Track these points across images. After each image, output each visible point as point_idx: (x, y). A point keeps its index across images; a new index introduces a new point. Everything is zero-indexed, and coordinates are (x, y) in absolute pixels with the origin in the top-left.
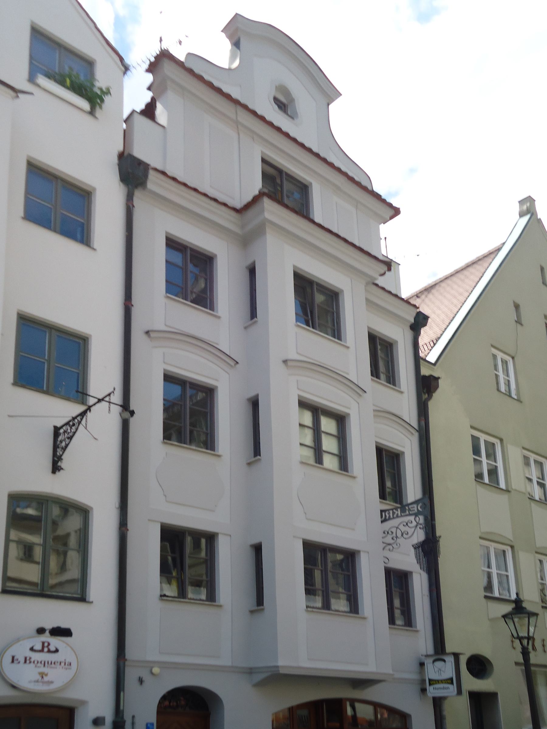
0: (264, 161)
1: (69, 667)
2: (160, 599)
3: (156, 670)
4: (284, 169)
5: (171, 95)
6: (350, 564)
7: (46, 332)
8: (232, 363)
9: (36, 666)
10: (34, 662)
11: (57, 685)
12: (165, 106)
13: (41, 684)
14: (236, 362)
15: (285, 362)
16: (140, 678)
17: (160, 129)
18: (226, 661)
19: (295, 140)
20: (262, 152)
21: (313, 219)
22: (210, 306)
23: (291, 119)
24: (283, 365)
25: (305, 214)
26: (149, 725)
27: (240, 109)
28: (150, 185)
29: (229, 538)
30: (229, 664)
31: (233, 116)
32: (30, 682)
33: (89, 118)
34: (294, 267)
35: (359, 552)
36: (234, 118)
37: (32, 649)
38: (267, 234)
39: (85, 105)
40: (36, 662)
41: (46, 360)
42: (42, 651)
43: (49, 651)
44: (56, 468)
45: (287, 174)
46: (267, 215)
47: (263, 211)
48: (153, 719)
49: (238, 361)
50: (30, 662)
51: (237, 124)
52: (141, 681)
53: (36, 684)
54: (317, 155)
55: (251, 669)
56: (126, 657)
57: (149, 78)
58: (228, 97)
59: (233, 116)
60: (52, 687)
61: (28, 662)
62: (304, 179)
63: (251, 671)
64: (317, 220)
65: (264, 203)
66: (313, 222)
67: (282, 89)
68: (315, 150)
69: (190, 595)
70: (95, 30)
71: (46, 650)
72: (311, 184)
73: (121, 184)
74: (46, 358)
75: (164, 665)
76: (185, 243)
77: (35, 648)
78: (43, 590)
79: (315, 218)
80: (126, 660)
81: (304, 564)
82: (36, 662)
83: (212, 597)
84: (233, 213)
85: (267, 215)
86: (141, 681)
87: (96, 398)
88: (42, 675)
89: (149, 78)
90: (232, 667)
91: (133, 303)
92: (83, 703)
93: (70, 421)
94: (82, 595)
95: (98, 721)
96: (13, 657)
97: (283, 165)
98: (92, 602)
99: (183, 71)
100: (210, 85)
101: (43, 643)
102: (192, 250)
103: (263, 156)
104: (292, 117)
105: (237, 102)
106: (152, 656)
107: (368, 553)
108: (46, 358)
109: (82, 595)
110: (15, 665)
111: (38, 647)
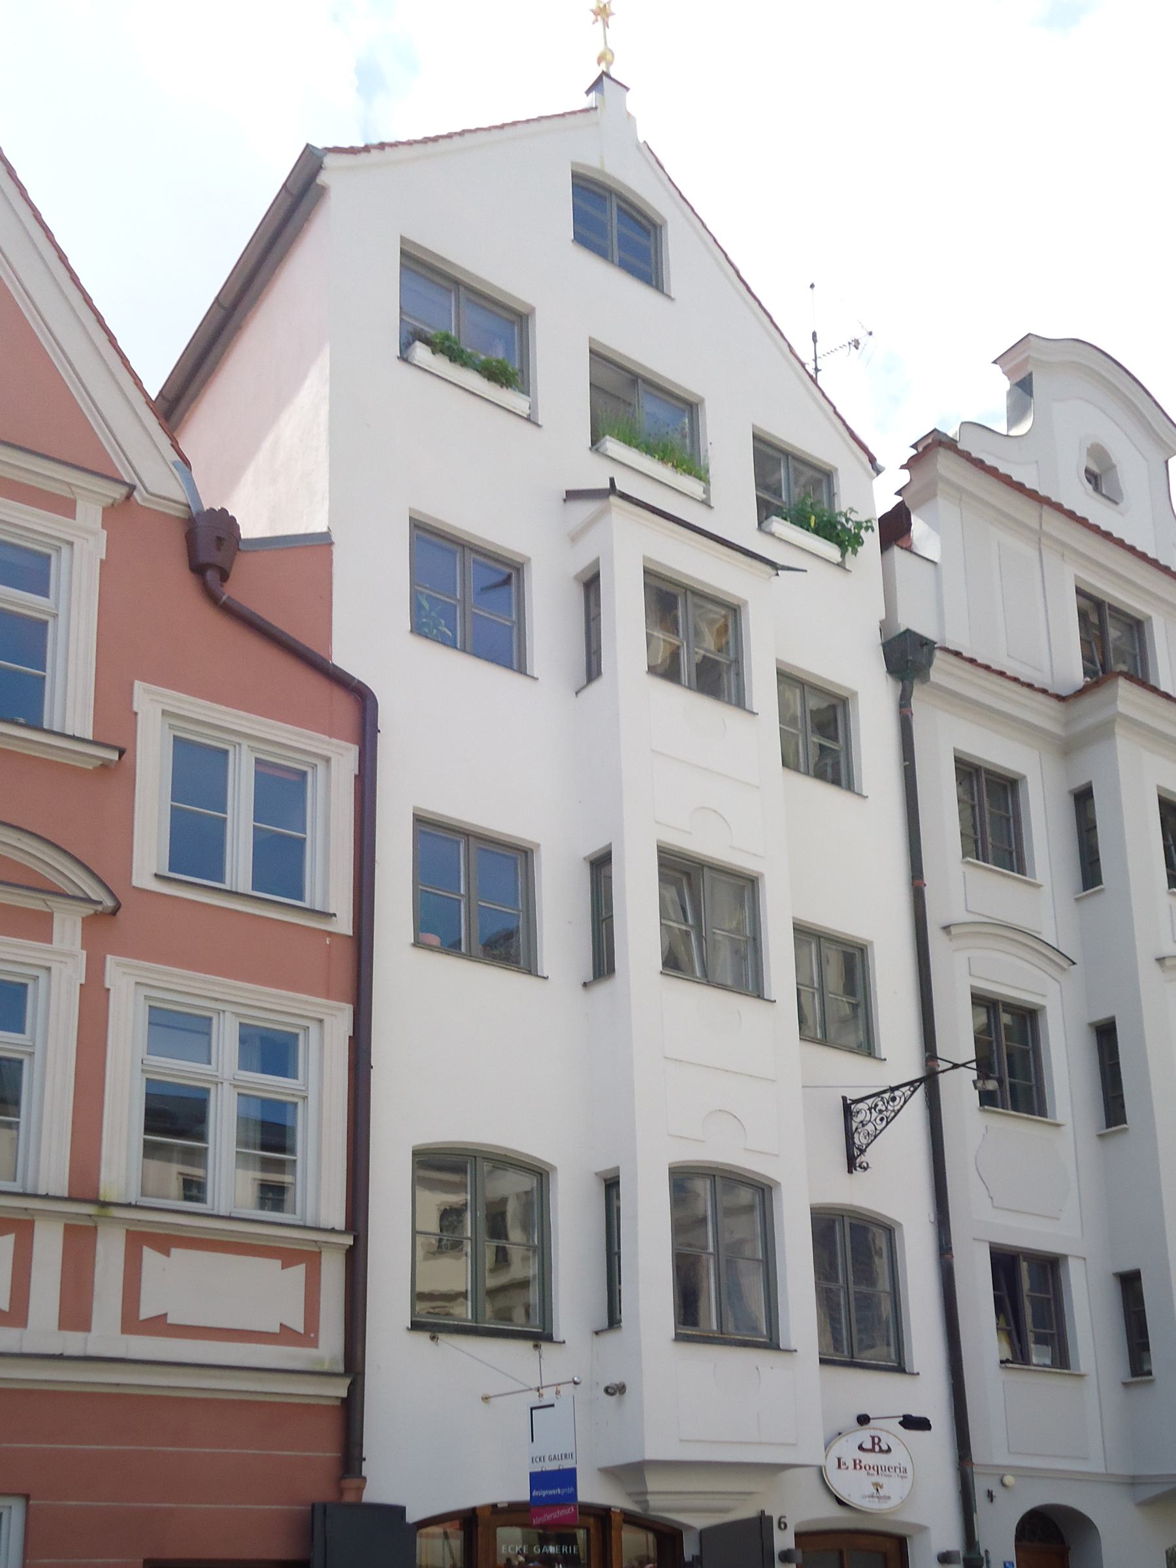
0: (1079, 592)
1: (905, 1474)
2: (1001, 1367)
3: (1009, 1480)
4: (1107, 600)
5: (944, 506)
6: (1050, 1283)
7: (458, 843)
8: (1064, 963)
9: (868, 1474)
10: (865, 1468)
11: (895, 1501)
12: (934, 524)
13: (876, 1500)
14: (1071, 963)
15: (1160, 960)
16: (989, 1491)
17: (929, 566)
18: (1096, 1466)
19: (1120, 543)
20: (1077, 577)
21: (1157, 687)
22: (983, 855)
23: (1112, 505)
24: (1156, 966)
25: (1140, 676)
26: (1007, 1565)
27: (1048, 512)
28: (935, 675)
29: (1082, 1262)
30: (1102, 1470)
31: (1034, 524)
32: (864, 1497)
33: (837, 573)
34: (1159, 787)
35: (1065, 1257)
36: (1038, 527)
37: (861, 1448)
38: (1116, 736)
39: (831, 551)
40: (867, 1468)
41: (462, 895)
42: (872, 1450)
43: (881, 1451)
44: (852, 1164)
45: (1111, 607)
46: (1122, 707)
47: (1114, 700)
48: (1011, 1556)
49: (1075, 961)
50: (861, 1467)
51: (1039, 537)
52: (990, 1495)
53: (871, 1499)
54: (1154, 563)
55: (1133, 1477)
56: (974, 1460)
57: (905, 477)
58: (1019, 487)
59: (1034, 524)
60: (884, 1506)
61: (858, 1467)
62: (1137, 610)
63: (1133, 1482)
64: (1163, 688)
65: (1117, 688)
66: (1155, 690)
67: (1098, 452)
68: (1151, 554)
69: (1035, 1360)
70: (834, 417)
71: (877, 1448)
72: (1150, 618)
73: (889, 678)
74: (462, 892)
75: (1019, 1471)
76: (977, 762)
77: (864, 1446)
78: (852, 1357)
79: (1161, 683)
80: (973, 1464)
81: (994, 1290)
82: (867, 1468)
83: (1062, 1360)
84: (1053, 703)
85: (1122, 707)
86: (990, 1495)
87: (950, 1062)
88: (878, 1487)
89: (905, 477)
90: (1107, 1474)
91: (926, 881)
92: (922, 1529)
93: (884, 1092)
94: (900, 1364)
95: (945, 1558)
96: (839, 1460)
97: (1104, 592)
98: (918, 1374)
99: (968, 465)
100: (979, 464)
101: (873, 1438)
102: (988, 772)
103: (1079, 586)
104: (1113, 500)
105: (1032, 495)
106: (1001, 1458)
107: (1085, 1259)
108: (462, 892)
109: (900, 1364)
110: (843, 1472)
111: (868, 1445)
